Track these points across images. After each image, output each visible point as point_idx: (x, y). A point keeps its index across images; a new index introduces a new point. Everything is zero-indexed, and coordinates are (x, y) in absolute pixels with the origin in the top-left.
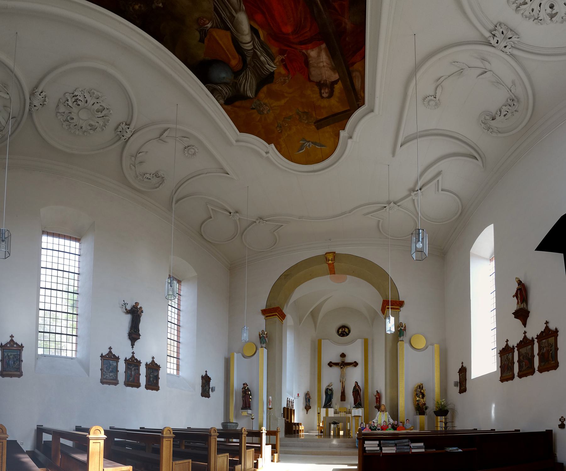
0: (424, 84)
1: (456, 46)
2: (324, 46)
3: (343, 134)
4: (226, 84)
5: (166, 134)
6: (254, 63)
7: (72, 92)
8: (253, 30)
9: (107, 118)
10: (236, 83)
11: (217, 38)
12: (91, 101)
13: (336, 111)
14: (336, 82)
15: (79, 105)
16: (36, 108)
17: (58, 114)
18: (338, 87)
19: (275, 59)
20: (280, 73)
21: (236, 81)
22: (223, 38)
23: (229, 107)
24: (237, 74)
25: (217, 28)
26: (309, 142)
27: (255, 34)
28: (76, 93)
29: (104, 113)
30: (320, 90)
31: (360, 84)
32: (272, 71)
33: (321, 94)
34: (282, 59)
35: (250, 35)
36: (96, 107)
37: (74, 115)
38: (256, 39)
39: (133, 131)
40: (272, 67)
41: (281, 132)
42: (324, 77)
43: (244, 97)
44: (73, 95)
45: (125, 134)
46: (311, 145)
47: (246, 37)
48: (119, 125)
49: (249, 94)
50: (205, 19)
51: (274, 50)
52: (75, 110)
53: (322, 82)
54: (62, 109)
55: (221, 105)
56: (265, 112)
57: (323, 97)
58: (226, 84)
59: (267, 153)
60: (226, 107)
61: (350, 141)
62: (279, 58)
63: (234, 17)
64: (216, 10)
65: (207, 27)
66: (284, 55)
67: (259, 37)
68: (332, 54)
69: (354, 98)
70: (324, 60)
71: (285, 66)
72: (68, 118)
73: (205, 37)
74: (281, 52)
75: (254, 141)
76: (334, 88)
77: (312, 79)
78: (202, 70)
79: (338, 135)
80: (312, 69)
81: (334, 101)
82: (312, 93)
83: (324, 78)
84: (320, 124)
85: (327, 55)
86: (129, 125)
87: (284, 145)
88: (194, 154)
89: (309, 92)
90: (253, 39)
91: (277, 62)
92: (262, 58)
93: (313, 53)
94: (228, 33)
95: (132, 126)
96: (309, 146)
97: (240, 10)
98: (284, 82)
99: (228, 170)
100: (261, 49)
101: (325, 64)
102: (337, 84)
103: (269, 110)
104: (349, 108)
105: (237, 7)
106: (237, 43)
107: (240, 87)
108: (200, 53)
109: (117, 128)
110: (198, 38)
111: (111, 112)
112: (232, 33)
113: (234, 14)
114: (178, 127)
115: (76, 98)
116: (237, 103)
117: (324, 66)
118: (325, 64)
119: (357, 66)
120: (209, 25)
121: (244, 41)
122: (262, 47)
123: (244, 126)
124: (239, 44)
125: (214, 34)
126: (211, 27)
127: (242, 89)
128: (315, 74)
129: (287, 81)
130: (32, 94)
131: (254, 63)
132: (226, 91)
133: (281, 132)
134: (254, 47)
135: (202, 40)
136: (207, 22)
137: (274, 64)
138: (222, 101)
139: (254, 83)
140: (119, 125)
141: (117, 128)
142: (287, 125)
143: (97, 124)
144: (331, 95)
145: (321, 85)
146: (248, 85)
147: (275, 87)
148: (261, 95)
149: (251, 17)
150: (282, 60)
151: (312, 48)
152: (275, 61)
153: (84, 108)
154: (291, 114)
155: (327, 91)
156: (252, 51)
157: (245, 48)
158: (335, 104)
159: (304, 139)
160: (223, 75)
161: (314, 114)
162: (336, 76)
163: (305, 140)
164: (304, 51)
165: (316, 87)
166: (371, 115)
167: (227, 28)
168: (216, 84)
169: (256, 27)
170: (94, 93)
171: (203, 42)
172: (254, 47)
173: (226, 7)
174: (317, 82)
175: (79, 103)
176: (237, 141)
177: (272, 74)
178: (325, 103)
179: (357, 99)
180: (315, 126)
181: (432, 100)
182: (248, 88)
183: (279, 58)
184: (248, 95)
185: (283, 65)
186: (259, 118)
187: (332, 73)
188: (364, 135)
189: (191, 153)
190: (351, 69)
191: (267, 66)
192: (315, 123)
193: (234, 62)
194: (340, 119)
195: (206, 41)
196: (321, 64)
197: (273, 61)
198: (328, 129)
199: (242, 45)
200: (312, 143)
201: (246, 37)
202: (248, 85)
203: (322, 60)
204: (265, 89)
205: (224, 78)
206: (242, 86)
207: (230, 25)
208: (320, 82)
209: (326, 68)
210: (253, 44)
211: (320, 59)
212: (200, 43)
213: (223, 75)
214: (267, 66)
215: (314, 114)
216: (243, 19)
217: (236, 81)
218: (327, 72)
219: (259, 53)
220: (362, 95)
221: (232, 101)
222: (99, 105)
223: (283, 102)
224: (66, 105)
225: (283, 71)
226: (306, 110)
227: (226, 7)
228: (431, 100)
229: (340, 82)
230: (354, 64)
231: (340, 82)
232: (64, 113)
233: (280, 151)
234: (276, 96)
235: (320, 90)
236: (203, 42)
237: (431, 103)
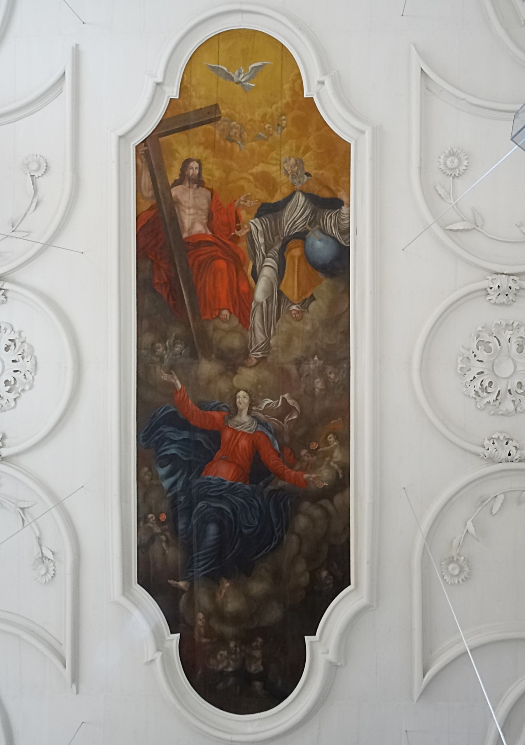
0: (55, 188)
1: (17, 267)
2: (185, 235)
3: (173, 92)
4: (323, 231)
5: (459, 226)
6: (274, 239)
7: (474, 400)
8: (256, 278)
9: (493, 330)
10: (310, 224)
11: (296, 290)
12: (478, 367)
13: (181, 136)
14: (177, 183)
15: (491, 383)
16: (513, 451)
17: (519, 409)
18: (174, 175)
19: (248, 233)
20: (248, 213)
21: (309, 228)
22: (291, 286)
23: (341, 195)
24: (302, 236)
25: (288, 299)
26: (239, 83)
27: (256, 272)
28: (473, 394)
29: (487, 338)
30: (200, 174)
31: (143, 181)
32: (257, 219)
33: (200, 168)
34: (238, 230)
35: (262, 274)
36: (482, 355)
37: (513, 384)
38: (258, 266)
39: (490, 278)
40: (255, 225)
41: (281, 116)
42: (191, 193)
43: (311, 197)
44: (477, 398)
45: (504, 287)
46: (235, 76)
47: (267, 273)
48: (495, 303)
49: (301, 199)
50: (294, 316)
51: (243, 245)
52: (502, 386)
53: (195, 185)
54: (508, 405)
55: (349, 206)
56: (292, 160)
57: (199, 161)
58: (323, 231)
59: (323, 83)
60: (345, 199)
61: (160, 79)
62: (242, 233)
63: (267, 300)
64: (278, 318)
65: (298, 307)
66: (235, 235)
67: (254, 267)
68: (175, 221)
69: (151, 155)
70: (187, 217)
71: (238, 219)
72: (520, 391)
73: (306, 299)
74: (236, 239)
75: (336, 117)
76: (180, 175)
77: (209, 193)
78: (337, 267)
79: (183, 89)
80: (205, 207)
81: (183, 153)
82: (213, 172)
83: (191, 191)
84: (210, 115)
85: (183, 223)
86: (486, 289)
87: (287, 86)
88: (452, 154)
89: (217, 174)
90: (261, 267)
91: (246, 229)
92: (262, 240)
93: (199, 228)
94: (282, 288)
95: (485, 284)
96: (240, 74)
97: (258, 303)
98: (247, 197)
99: (416, 75)
100: (258, 252)
101: (187, 211)
102: (175, 181)
103: (286, 162)
104: (161, 139)
105: (259, 308)
106: (280, 274)
107: (307, 216)
108: (324, 287)
109: (503, 304)
110: (313, 303)
111: (480, 329)
112: (278, 287)
113: (265, 302)
114: (430, 220)
115: (480, 392)
116: (326, 194)
117: (189, 208)
118: (187, 211)
119: (146, 205)
120: (294, 307)
121: (271, 270)
122: (255, 253)
123: (336, 153)
124: (279, 270)
125: (296, 296)
126: (294, 304)
127: (308, 212)
128: (203, 199)
129: (242, 198)
130: (491, 460)
131: (274, 239)
132: (329, 221)
133: (282, 115)
134: (264, 258)
135: (312, 298)
136: (293, 312)
137: (250, 228)
138: (344, 209)
139: (286, 213)
140: (495, 303)
141: (503, 304)
142: (267, 126)
143: (513, 340)
144: (186, 163)
145: (199, 182)
146: (297, 212)
147: (262, 196)
148: (286, 191)
149: (252, 291)
150: (239, 229)
151: (199, 235)
152: (248, 230)
153: (493, 371)
154: (254, 143)
155: (191, 172)
156: (269, 254)
157: (274, 262)
158: (183, 148)
159: (246, 89)
160: (319, 244)
161: (218, 136)
162: (175, 192)
163: (243, 86)
164: (210, 233)
165: (205, 180)
166: (122, 131)
167: (280, 293)
168: (335, 239)
169: (251, 279)
170: (462, 369)
171: (312, 295)
172: (264, 258)
173: (268, 314)
174: (203, 187)
175: (486, 384)
176: (363, 132)
177: (258, 216)
178: (197, 152)
179: (147, 154)
180: (220, 112)
181: (38, 170)
182: (299, 208)
183: (242, 233)
184: (304, 199)
185: (239, 222)
186: (308, 155)
187: (179, 197)
188: (132, 96)
189: (456, 161)
190: (154, 201)
191: (260, 228)
192: (219, 118)
193: (297, 252)
194: (178, 121)
195: (309, 294)
196: (192, 211)
197: (251, 232)
198: (199, 104)
199: (276, 266)
200: (232, 79)
201: (267, 273)
202: (297, 212)
203: (191, 217)
204: (278, 197)
205: (320, 240)
206: (304, 216)
207: (276, 295)
208: (198, 187)
209: (187, 205)
210: (263, 262)
211: (192, 220)
212: (316, 297)
213: (319, 244)
214: (260, 228)
215: (218, 136)
216: (259, 295)
217: (309, 228)
218: (186, 199)
219: (263, 248)
220: (139, 161)
221: (330, 202)
222: (476, 352)
223: (259, 168)
224: (497, 403)
225: (243, 214)
226: (229, 144)
227: (268, 314)
228: (38, 170)
229: (171, 182)
230: (150, 209)
231: (171, 182)
232: (513, 401)
233: (299, 75)
234: (266, 182)
235: (200, 174)
236: (312, 295)
237: (34, 166)
